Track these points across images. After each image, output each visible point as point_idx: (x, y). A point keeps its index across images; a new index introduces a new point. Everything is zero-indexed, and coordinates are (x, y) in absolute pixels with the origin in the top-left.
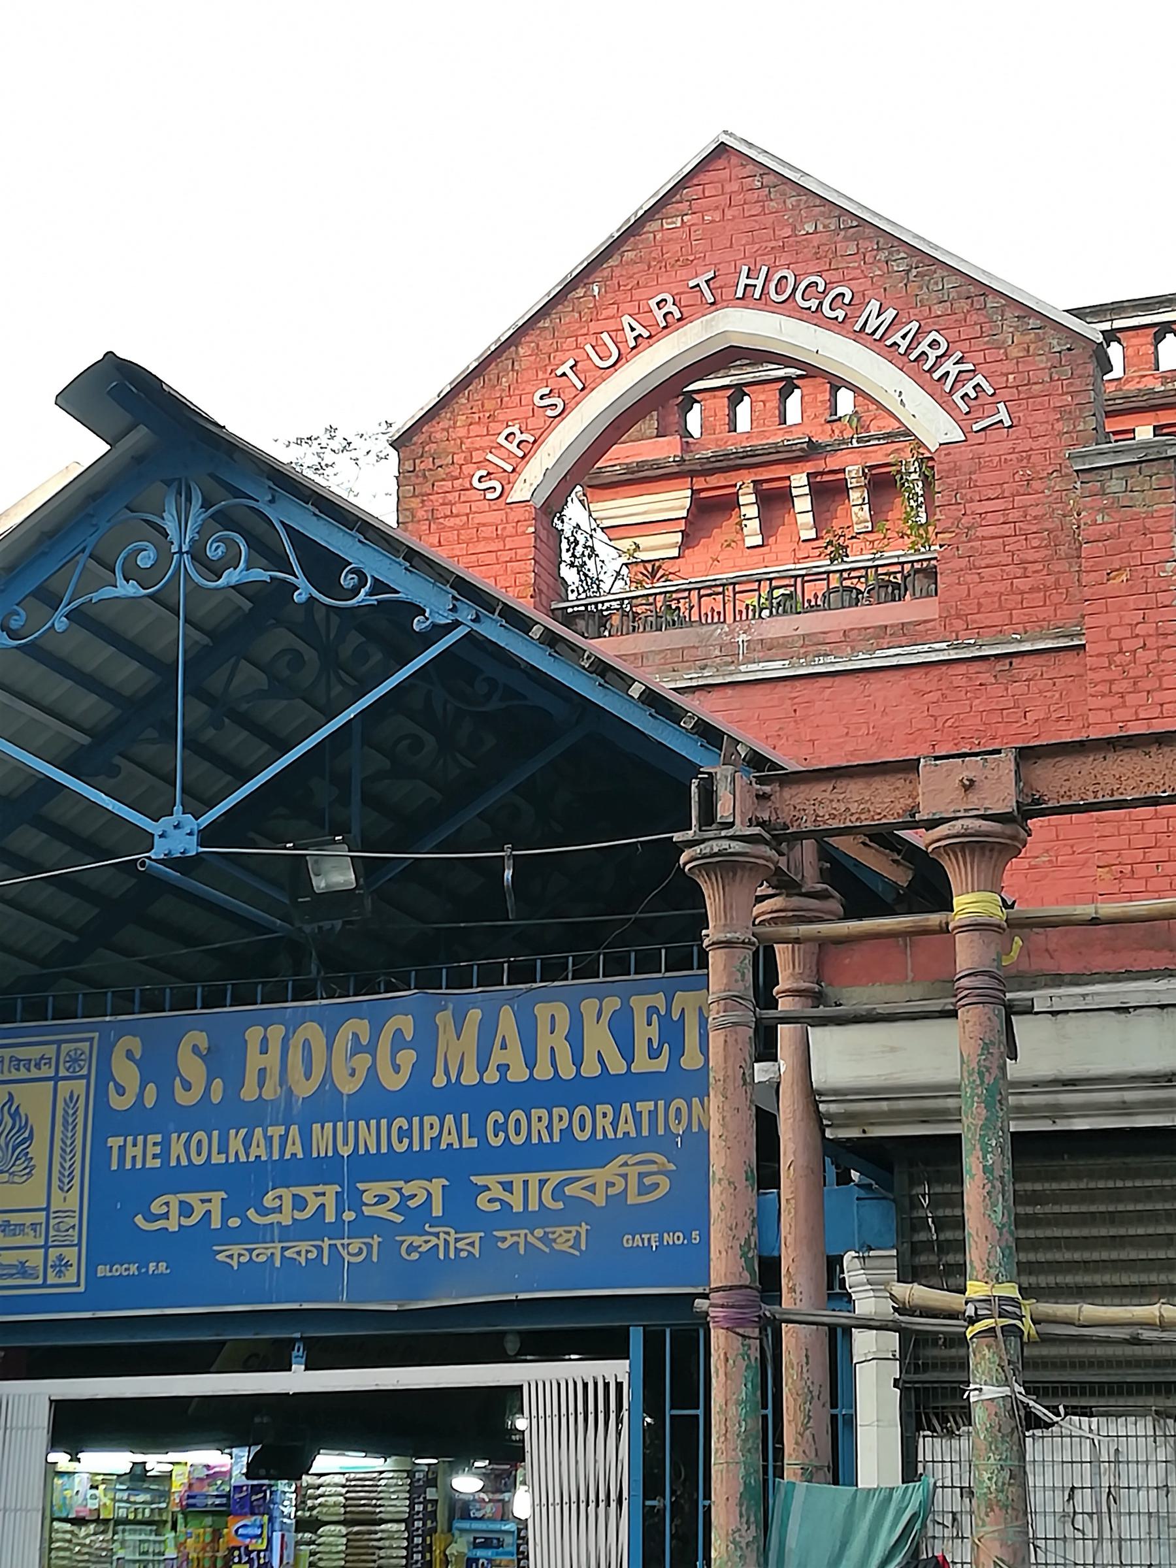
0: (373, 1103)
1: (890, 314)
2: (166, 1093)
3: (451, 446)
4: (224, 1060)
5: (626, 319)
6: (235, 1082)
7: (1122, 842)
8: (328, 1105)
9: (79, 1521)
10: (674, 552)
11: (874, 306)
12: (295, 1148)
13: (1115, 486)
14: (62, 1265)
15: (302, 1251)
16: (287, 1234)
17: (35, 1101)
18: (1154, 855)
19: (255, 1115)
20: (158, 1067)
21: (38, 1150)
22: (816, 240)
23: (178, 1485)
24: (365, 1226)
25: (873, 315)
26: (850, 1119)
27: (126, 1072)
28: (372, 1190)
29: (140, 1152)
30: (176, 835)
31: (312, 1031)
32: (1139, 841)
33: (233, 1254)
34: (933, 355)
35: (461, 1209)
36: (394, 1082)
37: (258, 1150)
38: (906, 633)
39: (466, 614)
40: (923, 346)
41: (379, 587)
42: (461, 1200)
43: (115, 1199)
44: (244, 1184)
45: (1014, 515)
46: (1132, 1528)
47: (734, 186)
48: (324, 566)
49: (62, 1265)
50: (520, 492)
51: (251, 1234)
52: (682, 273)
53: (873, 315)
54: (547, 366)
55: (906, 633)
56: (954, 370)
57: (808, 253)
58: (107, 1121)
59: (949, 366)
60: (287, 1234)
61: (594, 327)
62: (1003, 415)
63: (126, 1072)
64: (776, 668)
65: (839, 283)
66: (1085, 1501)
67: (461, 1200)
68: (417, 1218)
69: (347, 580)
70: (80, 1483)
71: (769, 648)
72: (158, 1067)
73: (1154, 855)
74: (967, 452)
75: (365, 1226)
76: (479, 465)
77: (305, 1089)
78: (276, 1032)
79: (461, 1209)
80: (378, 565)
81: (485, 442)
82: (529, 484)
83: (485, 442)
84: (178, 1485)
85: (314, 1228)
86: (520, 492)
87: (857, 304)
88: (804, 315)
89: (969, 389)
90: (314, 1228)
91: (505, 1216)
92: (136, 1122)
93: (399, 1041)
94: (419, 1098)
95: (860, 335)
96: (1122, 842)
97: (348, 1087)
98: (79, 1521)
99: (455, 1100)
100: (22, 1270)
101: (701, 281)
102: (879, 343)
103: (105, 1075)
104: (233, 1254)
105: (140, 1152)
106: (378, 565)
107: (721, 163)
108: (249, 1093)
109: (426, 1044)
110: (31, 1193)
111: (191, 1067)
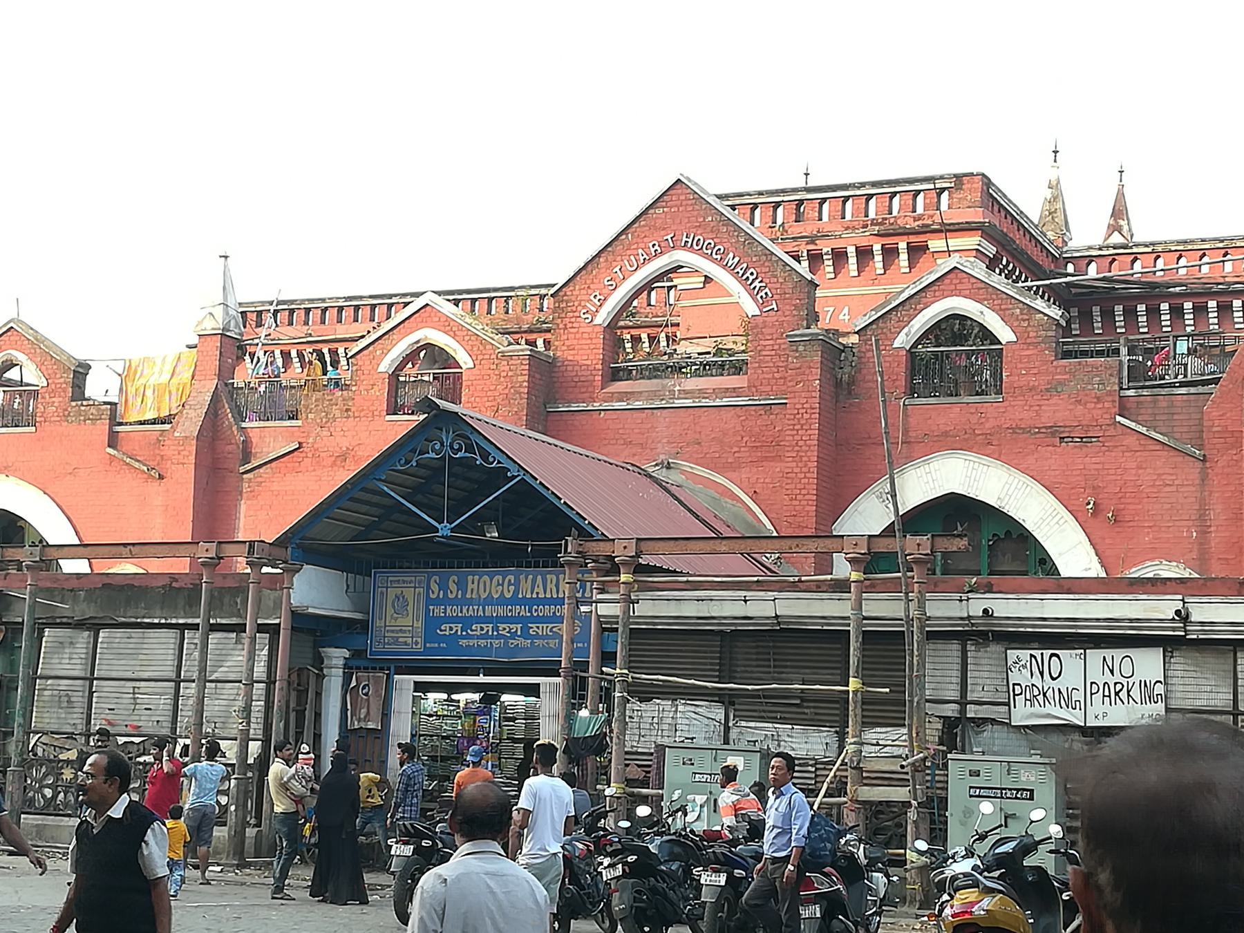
0: (502, 601)
1: (737, 259)
2: (445, 594)
3: (573, 298)
4: (462, 585)
5: (640, 251)
6: (464, 594)
7: (793, 486)
8: (489, 601)
9: (430, 716)
10: (701, 285)
11: (731, 255)
12: (481, 613)
13: (801, 348)
14: (417, 643)
15: (482, 642)
16: (478, 637)
17: (409, 593)
18: (803, 492)
19: (470, 602)
20: (443, 586)
21: (410, 608)
22: (712, 224)
23: (462, 705)
24: (499, 637)
25: (731, 260)
26: (606, 623)
27: (435, 587)
28: (501, 626)
29: (438, 611)
30: (444, 529)
31: (486, 578)
32: (799, 486)
33: (463, 642)
34: (751, 278)
35: (525, 634)
36: (508, 596)
37: (471, 613)
38: (735, 392)
39: (522, 473)
40: (748, 274)
41: (499, 462)
42: (525, 630)
43: (432, 624)
44: (467, 622)
45: (776, 347)
46: (665, 727)
47: (683, 197)
48: (485, 455)
49: (417, 643)
50: (599, 320)
51: (468, 637)
52: (663, 233)
53: (731, 260)
54: (610, 267)
55: (735, 392)
56: (759, 285)
57: (709, 229)
58: (429, 601)
59: (756, 283)
60: (478, 637)
61: (629, 252)
62: (774, 306)
63: (435, 587)
64: (688, 402)
65: (720, 243)
66: (656, 720)
67: (525, 630)
68: (514, 635)
69: (491, 459)
70: (430, 702)
71: (686, 393)
72: (443, 586)
73: (803, 492)
74: (760, 319)
75: (499, 637)
76: (584, 307)
77: (484, 596)
78: (477, 577)
79: (525, 634)
80: (499, 456)
81: (586, 298)
82: (602, 318)
83: (586, 298)
84: (462, 705)
85: (485, 636)
86: (599, 320)
87: (725, 253)
88: (706, 256)
89: (763, 294)
90: (485, 636)
91: (537, 636)
92: (437, 602)
93: (510, 584)
94: (514, 601)
95: (725, 267)
96: (793, 486)
97: (496, 596)
98: (430, 716)
99: (524, 602)
100: (405, 643)
101: (669, 237)
102: (732, 270)
103: (429, 587)
104: (463, 642)
105: (438, 611)
106: (499, 456)
107: (678, 186)
108: (468, 596)
109: (517, 584)
110: (408, 621)
111: (453, 587)
